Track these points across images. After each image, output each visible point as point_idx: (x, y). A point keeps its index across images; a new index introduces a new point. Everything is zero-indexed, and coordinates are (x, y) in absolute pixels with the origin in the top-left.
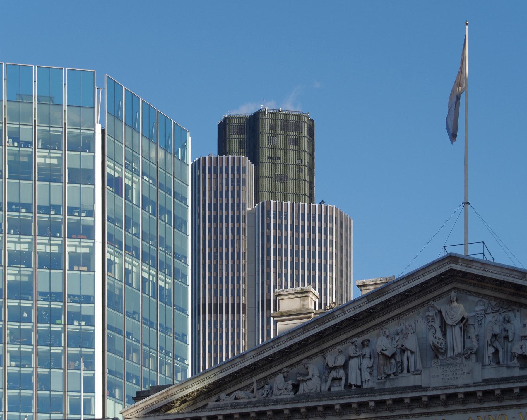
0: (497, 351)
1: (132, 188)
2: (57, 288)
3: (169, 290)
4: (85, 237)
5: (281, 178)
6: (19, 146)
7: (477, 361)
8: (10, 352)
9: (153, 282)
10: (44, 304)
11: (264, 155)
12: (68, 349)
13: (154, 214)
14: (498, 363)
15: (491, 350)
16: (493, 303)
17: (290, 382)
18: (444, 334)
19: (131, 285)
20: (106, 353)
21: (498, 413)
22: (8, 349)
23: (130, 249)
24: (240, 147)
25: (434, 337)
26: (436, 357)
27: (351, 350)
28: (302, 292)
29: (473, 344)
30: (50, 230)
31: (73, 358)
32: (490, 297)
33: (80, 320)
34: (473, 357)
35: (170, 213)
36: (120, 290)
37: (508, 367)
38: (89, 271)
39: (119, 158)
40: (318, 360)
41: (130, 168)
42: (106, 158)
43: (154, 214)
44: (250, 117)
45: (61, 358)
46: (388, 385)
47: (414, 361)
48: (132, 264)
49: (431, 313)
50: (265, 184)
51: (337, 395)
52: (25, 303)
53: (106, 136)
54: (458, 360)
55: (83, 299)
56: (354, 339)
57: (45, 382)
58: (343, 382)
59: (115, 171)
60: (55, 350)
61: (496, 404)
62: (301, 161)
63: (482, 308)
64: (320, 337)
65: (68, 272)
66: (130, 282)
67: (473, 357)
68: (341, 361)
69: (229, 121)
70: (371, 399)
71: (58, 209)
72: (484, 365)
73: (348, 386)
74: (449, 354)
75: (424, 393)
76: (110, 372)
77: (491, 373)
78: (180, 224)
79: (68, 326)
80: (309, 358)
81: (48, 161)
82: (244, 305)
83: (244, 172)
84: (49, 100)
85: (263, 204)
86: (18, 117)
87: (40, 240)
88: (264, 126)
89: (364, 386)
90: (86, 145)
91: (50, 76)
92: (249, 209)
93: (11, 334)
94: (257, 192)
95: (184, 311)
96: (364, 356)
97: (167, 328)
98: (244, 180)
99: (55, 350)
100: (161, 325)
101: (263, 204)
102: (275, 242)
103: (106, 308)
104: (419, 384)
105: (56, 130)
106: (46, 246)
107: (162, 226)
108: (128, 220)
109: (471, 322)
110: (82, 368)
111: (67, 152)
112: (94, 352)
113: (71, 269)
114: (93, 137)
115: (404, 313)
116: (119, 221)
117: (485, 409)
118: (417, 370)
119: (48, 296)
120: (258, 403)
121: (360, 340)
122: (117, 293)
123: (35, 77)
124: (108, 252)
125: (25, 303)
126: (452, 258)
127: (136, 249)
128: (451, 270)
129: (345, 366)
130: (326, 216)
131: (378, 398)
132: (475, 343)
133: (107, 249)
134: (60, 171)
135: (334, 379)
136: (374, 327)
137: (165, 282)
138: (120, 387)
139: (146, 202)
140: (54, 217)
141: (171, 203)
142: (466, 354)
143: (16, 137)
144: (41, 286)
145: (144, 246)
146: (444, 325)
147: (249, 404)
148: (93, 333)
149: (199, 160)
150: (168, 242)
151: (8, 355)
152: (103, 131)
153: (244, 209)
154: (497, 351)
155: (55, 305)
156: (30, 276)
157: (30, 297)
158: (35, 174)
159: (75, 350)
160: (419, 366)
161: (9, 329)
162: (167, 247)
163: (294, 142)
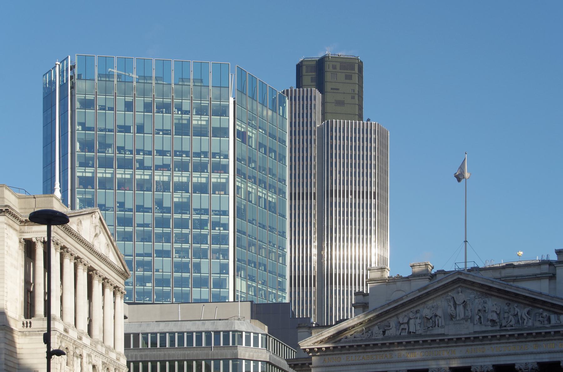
0: (480, 317)
1: (252, 137)
2: (205, 206)
3: (275, 203)
4: (223, 172)
5: (340, 103)
6: (182, 114)
7: (471, 322)
8: (175, 248)
9: (265, 198)
11: (328, 87)
12: (212, 246)
13: (265, 153)
14: (481, 323)
15: (478, 317)
16: (479, 293)
17: (381, 330)
18: (455, 308)
19: (251, 202)
20: (236, 248)
21: (481, 347)
22: (174, 246)
24: (312, 82)
25: (451, 310)
26: (452, 319)
27: (411, 315)
28: (382, 269)
29: (469, 314)
30: (200, 168)
31: (215, 251)
32: (477, 291)
33: (219, 227)
34: (469, 320)
35: (275, 152)
36: (245, 205)
37: (486, 326)
38: (225, 194)
39: (245, 120)
40: (395, 318)
41: (251, 125)
42: (236, 120)
43: (265, 153)
44: (319, 60)
45: (207, 251)
46: (428, 333)
47: (441, 321)
48: (251, 188)
49: (450, 298)
50: (329, 108)
51: (404, 337)
52: (185, 216)
53: (236, 105)
54: (462, 322)
55: (221, 213)
56: (412, 310)
57: (197, 267)
58: (407, 330)
59: (242, 127)
60: (204, 246)
61: (480, 343)
62: (354, 90)
63: (473, 296)
64: (395, 308)
65: (212, 195)
66: (251, 199)
67: (469, 320)
68: (406, 320)
69: (304, 63)
70: (420, 339)
71: (205, 154)
72: (474, 324)
73: (409, 333)
74: (458, 318)
75: (446, 337)
76: (238, 260)
77: (478, 328)
78: (282, 158)
79: (212, 231)
80: (390, 318)
81: (200, 122)
82: (315, 193)
83: (315, 100)
84: (200, 81)
85: (328, 122)
86: (181, 95)
87: (194, 174)
88: (328, 67)
89: (417, 333)
90: (223, 112)
91: (201, 67)
92: (318, 126)
93: (176, 236)
95: (284, 216)
96: (417, 318)
97: (273, 228)
98: (315, 105)
99: (204, 246)
100: (270, 227)
101: (328, 122)
102: (336, 149)
103: (236, 218)
104: (443, 332)
105: (205, 103)
106: (198, 178)
107: (270, 162)
108: (250, 158)
109: (468, 303)
110: (221, 258)
111: (212, 117)
112: (228, 248)
113: (214, 193)
114: (228, 106)
115: (436, 297)
116: (244, 160)
117: (475, 345)
118: (442, 326)
119: (200, 211)
120: (365, 340)
121: (415, 309)
122: (243, 207)
123: (192, 68)
124: (237, 181)
125: (185, 216)
126: (459, 272)
127: (254, 178)
128: (459, 278)
129: (408, 323)
130: (371, 130)
131: (424, 339)
132: (470, 314)
133: (237, 179)
134: (207, 128)
135: (402, 329)
136: (422, 304)
137: (272, 198)
138: (245, 270)
139: (261, 145)
140: (204, 159)
141: (276, 145)
142: (466, 319)
143: (179, 108)
144: (195, 205)
145: (259, 175)
146: (455, 304)
147: (361, 340)
148: (228, 235)
149: (284, 91)
150: (274, 172)
151: (174, 250)
152: (234, 102)
153: (315, 126)
154: (480, 317)
155: (204, 217)
156: (188, 198)
157: (188, 213)
158: (191, 132)
159: (217, 246)
160: (443, 324)
161: (175, 233)
162: (273, 175)
163: (349, 77)
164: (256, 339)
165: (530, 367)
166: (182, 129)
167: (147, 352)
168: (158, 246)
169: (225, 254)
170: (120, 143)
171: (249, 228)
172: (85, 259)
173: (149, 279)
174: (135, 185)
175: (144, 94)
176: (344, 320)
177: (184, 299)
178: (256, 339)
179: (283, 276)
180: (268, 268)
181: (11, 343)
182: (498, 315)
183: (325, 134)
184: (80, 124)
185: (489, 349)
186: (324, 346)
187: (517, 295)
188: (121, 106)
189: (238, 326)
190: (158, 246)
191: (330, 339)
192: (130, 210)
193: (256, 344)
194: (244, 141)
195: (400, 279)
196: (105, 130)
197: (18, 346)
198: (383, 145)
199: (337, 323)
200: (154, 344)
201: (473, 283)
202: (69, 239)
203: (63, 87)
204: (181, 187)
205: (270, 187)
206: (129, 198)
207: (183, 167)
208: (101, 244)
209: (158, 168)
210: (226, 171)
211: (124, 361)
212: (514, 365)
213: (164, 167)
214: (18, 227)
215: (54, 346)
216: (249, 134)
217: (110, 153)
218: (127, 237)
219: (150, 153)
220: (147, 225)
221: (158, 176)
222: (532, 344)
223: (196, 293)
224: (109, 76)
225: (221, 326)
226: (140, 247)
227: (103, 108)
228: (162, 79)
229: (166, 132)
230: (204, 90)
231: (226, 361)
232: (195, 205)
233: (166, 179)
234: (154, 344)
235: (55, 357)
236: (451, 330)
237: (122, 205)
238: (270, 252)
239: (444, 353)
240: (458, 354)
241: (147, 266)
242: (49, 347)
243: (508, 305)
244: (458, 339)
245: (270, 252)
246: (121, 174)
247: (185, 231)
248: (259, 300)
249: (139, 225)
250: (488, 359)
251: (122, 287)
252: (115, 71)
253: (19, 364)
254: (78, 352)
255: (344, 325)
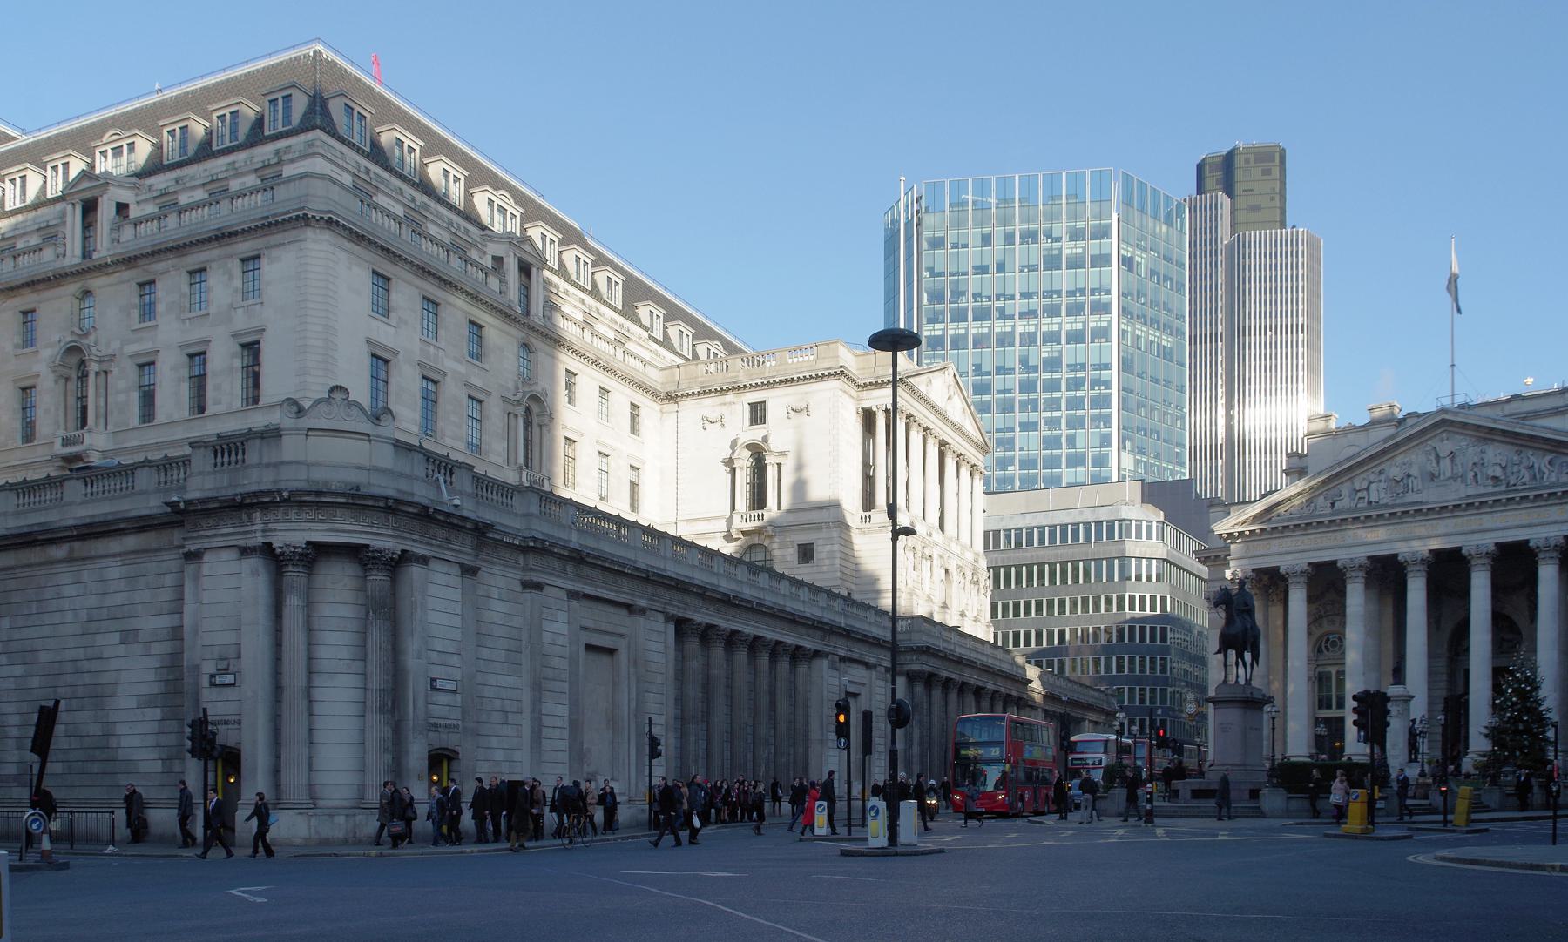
10: (1072, 375)
11: (1239, 188)
23: (1142, 318)
25: (1432, 466)
30: (1075, 310)
31: (1093, 419)
48: (1141, 330)
50: (1241, 217)
51: (1362, 510)
52: (1056, 375)
57: (1072, 441)
60: (1079, 413)
64: (1350, 469)
68: (1364, 485)
70: (1386, 512)
71: (1082, 292)
73: (1370, 503)
77: (1471, 491)
84: (1075, 196)
86: (1051, 217)
88: (1239, 162)
94: (1233, 226)
95: (1183, 365)
99: (1079, 413)
105: (1081, 225)
106: (1072, 324)
107: (1164, 293)
119: (1074, 367)
125: (1056, 375)
126: (1443, 410)
129: (1367, 489)
139: (1153, 273)
140: (1079, 298)
142: (1454, 478)
143: (1049, 235)
144: (1068, 359)
145: (1149, 312)
146: (1438, 458)
155: (1080, 374)
158: (1064, 264)
164: (1149, 529)
165: (1553, 543)
166: (1052, 262)
167: (1012, 554)
168: (1023, 417)
169: (1107, 420)
170: (974, 289)
171: (1137, 383)
172: (936, 431)
173: (1011, 461)
174: (994, 340)
175: (1005, 221)
176: (1271, 492)
177: (1054, 483)
178: (1149, 529)
179: (1182, 445)
180: (1162, 436)
181: (847, 543)
182: (1504, 468)
183: (1236, 253)
184: (927, 269)
185: (1488, 520)
186: (1247, 529)
187: (1532, 437)
188: (976, 240)
189: (1127, 512)
190: (1023, 417)
191: (1256, 519)
192: (989, 373)
193: (1149, 536)
194: (1130, 269)
195: (1352, 429)
196: (957, 274)
197: (856, 547)
198: (1314, 258)
199: (1263, 496)
200: (1018, 544)
201: (1465, 425)
202: (916, 404)
203: (909, 224)
204: (1052, 337)
205: (1166, 328)
206: (989, 357)
207: (1053, 311)
208: (957, 409)
209: (1022, 315)
210: (1108, 312)
211: (983, 564)
212: (1527, 541)
213: (1031, 314)
214: (854, 393)
215: (903, 520)
216: (1138, 259)
217: (964, 302)
218: (984, 409)
219: (1012, 297)
220: (1009, 391)
221: (1024, 327)
222: (1554, 509)
223: (1069, 475)
224: (964, 203)
225: (1104, 515)
226: (999, 419)
227: (955, 246)
228: (1027, 199)
229: (1032, 268)
230: (1079, 207)
231: (1110, 560)
232: (1068, 359)
233: (1032, 329)
234: (1018, 544)
235: (902, 538)
236: (1431, 496)
237: (978, 367)
238: (1165, 414)
239: (1419, 529)
240: (1441, 530)
241: (1008, 444)
242: (894, 524)
243: (1519, 453)
244: (1442, 508)
245: (1165, 414)
246: (977, 328)
247: (1056, 395)
248: (1149, 479)
249: (999, 392)
250: (1488, 535)
251: (981, 466)
252: (970, 197)
253: (857, 571)
254: (927, 552)
255: (1275, 498)
